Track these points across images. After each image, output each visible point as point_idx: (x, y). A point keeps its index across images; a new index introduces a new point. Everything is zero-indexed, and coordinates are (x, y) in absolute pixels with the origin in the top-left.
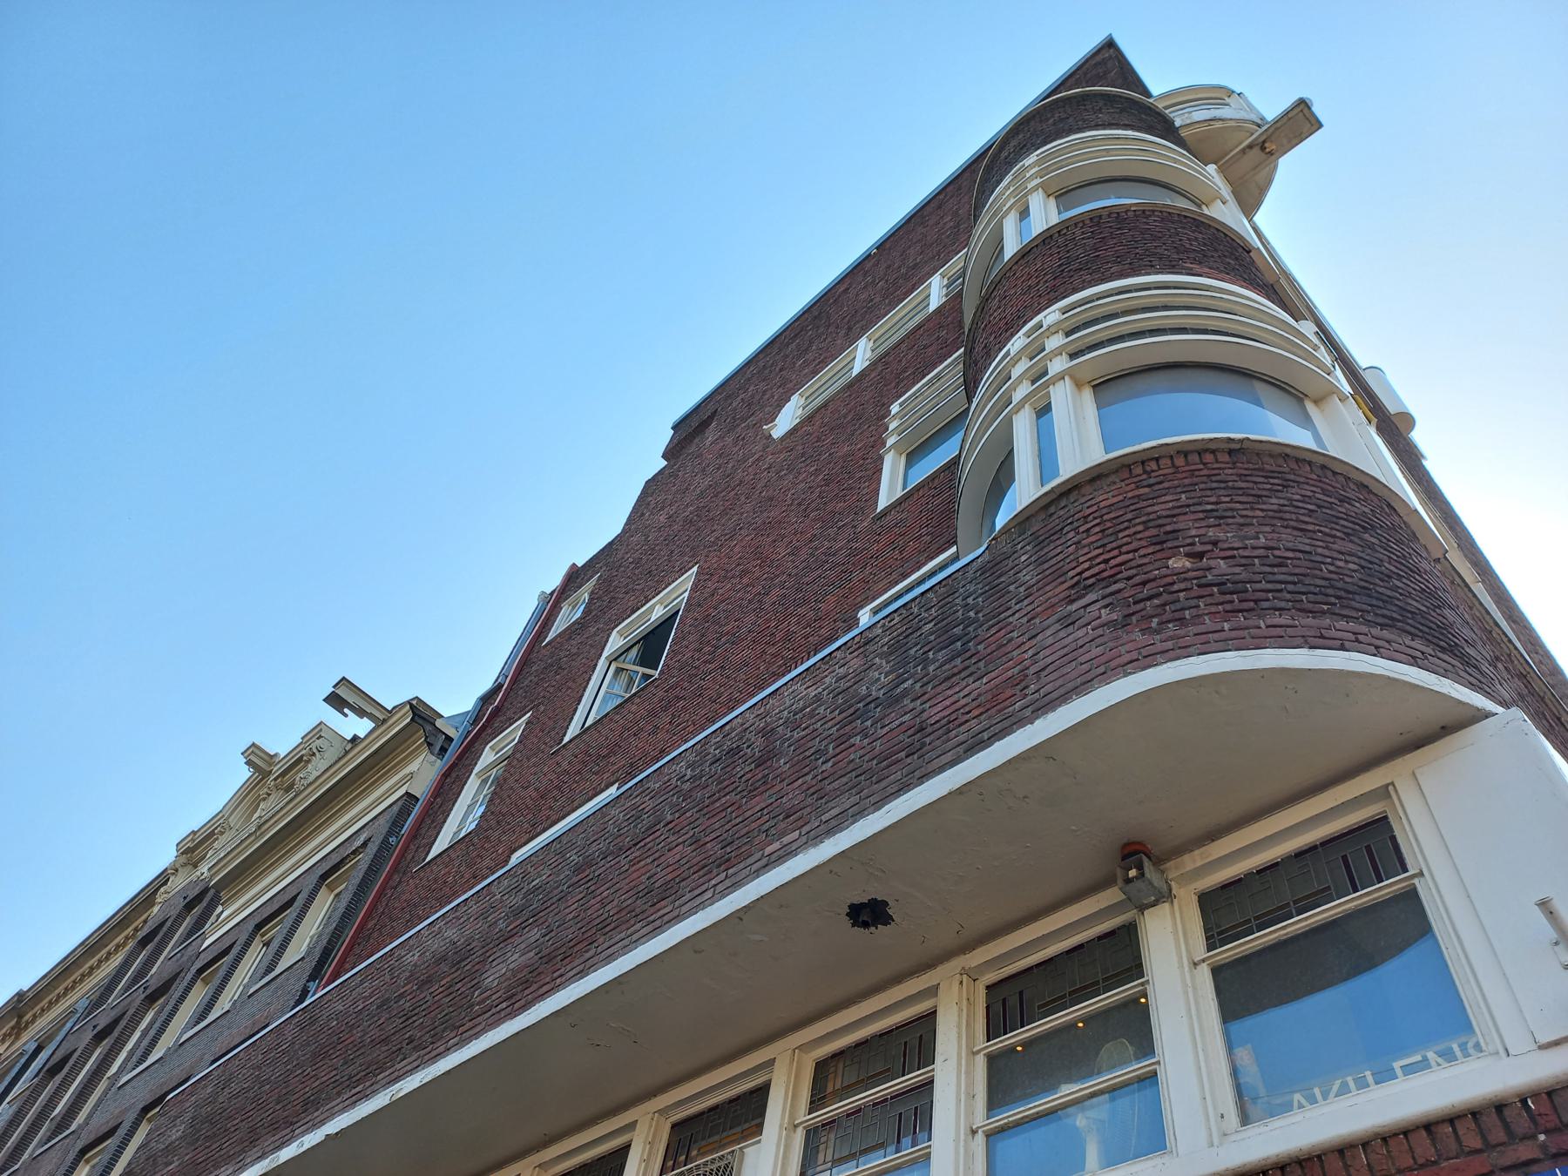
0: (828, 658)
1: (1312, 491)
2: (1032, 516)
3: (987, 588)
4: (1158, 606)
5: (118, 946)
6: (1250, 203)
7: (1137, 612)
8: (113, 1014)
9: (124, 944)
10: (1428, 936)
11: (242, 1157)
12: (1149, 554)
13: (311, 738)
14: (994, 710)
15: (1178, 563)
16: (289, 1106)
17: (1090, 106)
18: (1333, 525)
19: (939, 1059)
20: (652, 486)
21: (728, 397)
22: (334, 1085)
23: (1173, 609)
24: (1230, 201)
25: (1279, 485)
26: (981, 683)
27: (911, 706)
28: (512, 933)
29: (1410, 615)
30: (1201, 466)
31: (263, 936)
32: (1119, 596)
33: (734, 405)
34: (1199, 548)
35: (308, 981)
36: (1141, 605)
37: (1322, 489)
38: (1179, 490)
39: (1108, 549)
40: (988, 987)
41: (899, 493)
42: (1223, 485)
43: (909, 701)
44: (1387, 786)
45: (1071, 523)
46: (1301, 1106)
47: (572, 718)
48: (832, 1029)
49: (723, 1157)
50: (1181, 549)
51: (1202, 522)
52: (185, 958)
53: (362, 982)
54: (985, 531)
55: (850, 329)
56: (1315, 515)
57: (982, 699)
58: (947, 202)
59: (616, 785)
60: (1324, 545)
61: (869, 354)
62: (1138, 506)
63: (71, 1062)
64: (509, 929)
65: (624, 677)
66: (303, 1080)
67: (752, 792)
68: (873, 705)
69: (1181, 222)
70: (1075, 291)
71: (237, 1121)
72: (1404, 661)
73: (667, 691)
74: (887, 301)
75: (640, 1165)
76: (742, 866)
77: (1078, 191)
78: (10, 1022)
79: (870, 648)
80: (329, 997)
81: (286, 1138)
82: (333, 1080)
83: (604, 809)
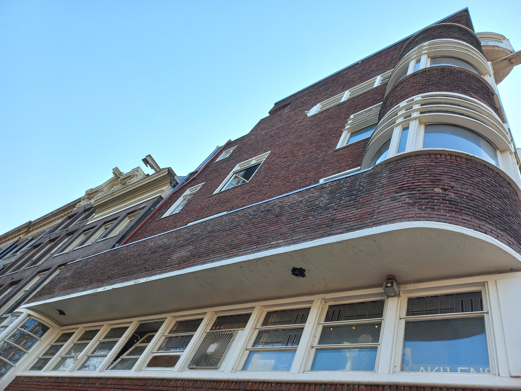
0: (308, 190)
1: (491, 180)
2: (391, 162)
3: (369, 181)
4: (427, 202)
5: (61, 217)
6: (499, 78)
7: (419, 202)
8: (56, 236)
9: (63, 217)
10: (484, 334)
11: (86, 287)
12: (428, 185)
13: (134, 171)
14: (360, 220)
15: (438, 190)
16: (103, 276)
17: (453, 30)
18: (495, 193)
19: (307, 322)
20: (262, 121)
21: (296, 99)
22: (118, 274)
23: (432, 204)
24: (492, 76)
25: (480, 174)
26: (358, 211)
27: (332, 212)
28: (184, 245)
29: (512, 230)
30: (455, 161)
31: (105, 226)
32: (414, 195)
33: (297, 102)
34: (446, 187)
35: (116, 243)
36: (421, 200)
37: (495, 180)
38: (445, 167)
39: (415, 179)
40: (329, 306)
41: (345, 145)
42: (461, 169)
43: (331, 210)
44: (485, 282)
45: (405, 168)
46: (422, 371)
47: (218, 187)
48: (276, 304)
49: (230, 331)
50: (440, 186)
51: (450, 179)
52: (81, 226)
53: (134, 247)
54: (373, 163)
55: (344, 86)
56: (489, 188)
57: (357, 216)
58: (390, 52)
59: (226, 212)
60: (490, 198)
61: (348, 96)
62: (429, 168)
63: (41, 246)
64: (184, 244)
65: (237, 180)
66: (110, 270)
67: (272, 224)
68: (319, 208)
69: (473, 78)
70: (429, 91)
71: (87, 276)
72: (506, 243)
73: (250, 188)
74: (360, 80)
75: (205, 325)
76: (262, 245)
77: (439, 58)
78: (26, 229)
79: (323, 190)
80: (123, 248)
81: (101, 285)
82: (118, 273)
83: (222, 217)
